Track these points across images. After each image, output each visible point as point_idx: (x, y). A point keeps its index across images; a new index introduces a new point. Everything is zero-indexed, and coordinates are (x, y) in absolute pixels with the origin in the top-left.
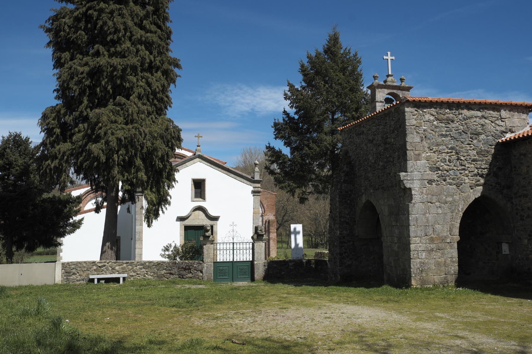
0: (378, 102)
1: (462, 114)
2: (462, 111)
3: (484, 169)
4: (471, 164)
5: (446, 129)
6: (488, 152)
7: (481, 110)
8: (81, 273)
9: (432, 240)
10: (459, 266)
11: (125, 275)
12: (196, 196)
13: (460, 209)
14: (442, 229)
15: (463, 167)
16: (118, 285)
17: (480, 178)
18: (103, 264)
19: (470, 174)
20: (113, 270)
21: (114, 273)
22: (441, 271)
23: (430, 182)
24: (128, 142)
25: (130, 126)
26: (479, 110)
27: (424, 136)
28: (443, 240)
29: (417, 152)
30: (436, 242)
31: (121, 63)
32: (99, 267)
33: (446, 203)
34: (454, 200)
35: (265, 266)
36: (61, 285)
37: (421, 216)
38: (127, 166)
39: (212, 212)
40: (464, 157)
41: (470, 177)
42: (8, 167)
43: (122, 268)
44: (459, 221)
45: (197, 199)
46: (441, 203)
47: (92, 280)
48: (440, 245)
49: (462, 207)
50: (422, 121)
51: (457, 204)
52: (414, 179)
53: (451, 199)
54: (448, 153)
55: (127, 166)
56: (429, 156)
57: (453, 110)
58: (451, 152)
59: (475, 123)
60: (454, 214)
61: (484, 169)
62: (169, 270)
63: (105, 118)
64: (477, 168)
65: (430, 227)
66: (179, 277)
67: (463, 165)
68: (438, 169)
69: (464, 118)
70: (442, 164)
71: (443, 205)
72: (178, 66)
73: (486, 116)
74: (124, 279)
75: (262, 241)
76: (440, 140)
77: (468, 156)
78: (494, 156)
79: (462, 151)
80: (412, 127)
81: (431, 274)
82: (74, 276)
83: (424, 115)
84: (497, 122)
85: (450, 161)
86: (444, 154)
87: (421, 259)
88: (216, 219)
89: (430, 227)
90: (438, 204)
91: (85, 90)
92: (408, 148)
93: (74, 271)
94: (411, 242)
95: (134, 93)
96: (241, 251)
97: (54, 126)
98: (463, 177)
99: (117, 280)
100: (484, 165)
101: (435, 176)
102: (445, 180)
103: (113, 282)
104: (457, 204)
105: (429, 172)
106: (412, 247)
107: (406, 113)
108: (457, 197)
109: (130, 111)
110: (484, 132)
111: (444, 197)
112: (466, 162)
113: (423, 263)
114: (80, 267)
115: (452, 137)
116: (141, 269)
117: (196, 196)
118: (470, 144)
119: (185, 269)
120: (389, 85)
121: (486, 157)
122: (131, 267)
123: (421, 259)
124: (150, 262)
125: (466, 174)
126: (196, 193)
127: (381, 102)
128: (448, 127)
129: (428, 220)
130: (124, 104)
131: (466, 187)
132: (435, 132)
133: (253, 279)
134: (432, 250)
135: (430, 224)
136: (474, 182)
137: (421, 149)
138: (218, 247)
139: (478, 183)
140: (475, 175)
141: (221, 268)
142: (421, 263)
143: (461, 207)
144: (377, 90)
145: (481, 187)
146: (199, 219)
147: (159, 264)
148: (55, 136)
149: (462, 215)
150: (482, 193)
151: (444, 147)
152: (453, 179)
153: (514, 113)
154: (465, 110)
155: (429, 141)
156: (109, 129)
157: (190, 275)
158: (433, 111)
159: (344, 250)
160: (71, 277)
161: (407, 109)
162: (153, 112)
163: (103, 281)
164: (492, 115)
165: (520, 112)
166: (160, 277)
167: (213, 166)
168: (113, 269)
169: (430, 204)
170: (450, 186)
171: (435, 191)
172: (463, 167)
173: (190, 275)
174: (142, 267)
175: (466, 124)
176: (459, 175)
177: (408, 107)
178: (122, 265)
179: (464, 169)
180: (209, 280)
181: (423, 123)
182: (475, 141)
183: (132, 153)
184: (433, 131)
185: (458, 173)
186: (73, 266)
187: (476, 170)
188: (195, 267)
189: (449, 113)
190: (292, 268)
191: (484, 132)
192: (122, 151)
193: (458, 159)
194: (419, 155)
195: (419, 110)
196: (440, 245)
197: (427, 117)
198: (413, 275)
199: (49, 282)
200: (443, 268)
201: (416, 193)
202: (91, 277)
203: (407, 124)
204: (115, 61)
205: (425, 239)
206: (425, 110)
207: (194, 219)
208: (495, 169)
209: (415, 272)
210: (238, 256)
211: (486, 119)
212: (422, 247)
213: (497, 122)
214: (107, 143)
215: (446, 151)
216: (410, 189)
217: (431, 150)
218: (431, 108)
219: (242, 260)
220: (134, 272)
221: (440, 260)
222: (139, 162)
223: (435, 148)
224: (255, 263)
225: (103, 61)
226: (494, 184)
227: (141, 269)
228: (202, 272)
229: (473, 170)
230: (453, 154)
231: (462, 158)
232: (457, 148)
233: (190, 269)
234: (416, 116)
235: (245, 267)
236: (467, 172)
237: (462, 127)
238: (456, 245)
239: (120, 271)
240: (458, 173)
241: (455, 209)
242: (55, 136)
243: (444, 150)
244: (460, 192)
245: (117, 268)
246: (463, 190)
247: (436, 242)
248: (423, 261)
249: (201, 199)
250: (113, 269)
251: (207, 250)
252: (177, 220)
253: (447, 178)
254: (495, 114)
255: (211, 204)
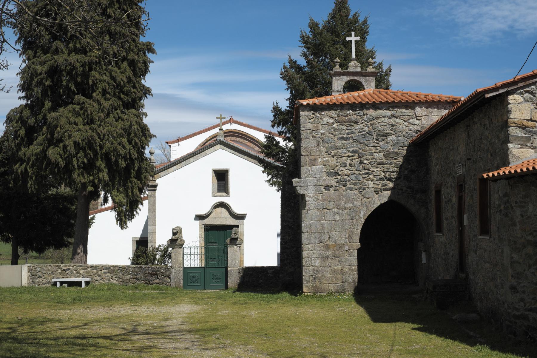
0: (334, 91)
1: (367, 114)
2: (368, 112)
3: (393, 172)
4: (377, 167)
5: (347, 131)
6: (397, 154)
7: (391, 109)
8: (47, 276)
9: (327, 247)
10: (358, 274)
11: (88, 279)
12: (219, 190)
13: (361, 216)
14: (339, 236)
15: (367, 171)
16: (79, 288)
17: (389, 182)
18: (67, 268)
19: (375, 179)
20: (78, 274)
21: (78, 277)
22: (337, 279)
23: (327, 188)
24: (86, 144)
25: (87, 127)
26: (388, 110)
27: (321, 141)
28: (340, 247)
29: (312, 157)
30: (332, 249)
31: (79, 60)
32: (64, 270)
33: (345, 209)
34: (355, 206)
35: (239, 273)
36: (27, 288)
37: (316, 222)
38: (89, 167)
39: (237, 210)
40: (368, 160)
41: (375, 182)
42: (6, 162)
43: (86, 272)
44: (360, 228)
45: (220, 194)
46: (339, 209)
47: (55, 284)
48: (337, 252)
49: (364, 214)
50: (319, 125)
51: (358, 210)
52: (309, 185)
53: (351, 205)
54: (349, 157)
55: (89, 167)
56: (326, 160)
57: (356, 111)
58: (352, 156)
59: (383, 124)
60: (355, 220)
61: (393, 172)
62: (135, 275)
63: (62, 121)
64: (384, 172)
65: (326, 234)
66: (146, 283)
67: (367, 169)
68: (337, 174)
69: (369, 119)
70: (342, 169)
71: (341, 211)
72: (152, 51)
73: (396, 115)
74: (87, 283)
75: (236, 245)
76: (339, 143)
77: (372, 159)
78: (406, 158)
79: (365, 154)
80: (308, 132)
81: (325, 282)
82: (40, 279)
83: (321, 119)
84: (411, 121)
85: (351, 165)
86: (344, 158)
87: (315, 266)
88: (242, 217)
89: (326, 234)
90: (335, 210)
91: (47, 90)
92: (302, 153)
93: (39, 274)
94: (304, 249)
95: (98, 89)
96: (193, 256)
97: (17, 129)
98: (366, 181)
99: (79, 284)
100: (393, 168)
101: (334, 182)
102: (344, 186)
103: (76, 286)
104: (358, 210)
105: (326, 177)
106: (305, 254)
107: (301, 118)
108: (358, 203)
109: (89, 112)
110: (393, 133)
111: (343, 203)
112: (370, 166)
113: (317, 271)
114: (45, 270)
115: (354, 140)
116: (106, 273)
117: (219, 190)
118: (376, 147)
119: (152, 275)
120: (353, 72)
121: (396, 159)
122: (95, 271)
123: (315, 266)
124: (115, 266)
125: (370, 178)
126: (219, 186)
127: (338, 91)
128: (350, 130)
129: (323, 227)
130: (84, 103)
131: (369, 192)
132: (334, 135)
133: (227, 287)
134: (327, 257)
135: (326, 231)
136: (380, 186)
137: (318, 153)
138: (185, 251)
139: (385, 187)
140: (382, 179)
141: (192, 274)
142: (314, 270)
143: (362, 213)
144: (334, 78)
145: (389, 192)
146: (222, 218)
147: (124, 269)
148: (19, 138)
149: (364, 221)
150: (390, 197)
151: (345, 151)
152: (355, 184)
153: (432, 110)
154: (371, 110)
155: (327, 145)
156: (66, 132)
157: (157, 281)
158: (333, 113)
159: (286, 257)
160: (37, 280)
161: (302, 113)
162: (119, 107)
163: (66, 285)
164: (404, 114)
165: (441, 108)
166: (126, 282)
167: (237, 153)
168: (78, 273)
169: (326, 210)
170: (351, 192)
171: (333, 197)
172: (367, 171)
173: (157, 281)
174: (107, 271)
175: (372, 125)
176: (362, 180)
177: (303, 111)
178: (86, 269)
179: (368, 173)
180: (177, 286)
181: (321, 127)
182: (382, 143)
183: (91, 155)
184: (332, 134)
185: (361, 177)
186: (38, 269)
187: (383, 174)
188: (163, 272)
189: (351, 114)
190: (271, 276)
191: (393, 133)
192: (81, 154)
193: (361, 163)
194: (315, 160)
195: (316, 114)
196: (337, 252)
197: (326, 120)
198: (305, 282)
199: (16, 284)
200: (340, 276)
201: (310, 199)
202: (54, 280)
203: (302, 129)
204: (74, 58)
205: (319, 247)
206: (322, 113)
207: (215, 218)
208: (406, 172)
209: (307, 279)
210: (189, 261)
211: (397, 118)
212: (317, 254)
213: (411, 121)
214: (65, 147)
215: (347, 155)
216: (303, 196)
217: (329, 154)
218: (330, 110)
219: (192, 266)
220: (99, 276)
221: (336, 268)
222: (100, 163)
223: (333, 153)
224: (229, 269)
225: (60, 59)
226: (404, 188)
227: (106, 273)
228: (170, 278)
229: (378, 173)
230: (356, 157)
231: (365, 162)
232: (360, 151)
233: (156, 274)
234: (312, 120)
235: (218, 274)
236: (371, 176)
237: (367, 129)
238: (356, 253)
239: (85, 275)
240: (361, 177)
241: (355, 216)
242: (19, 138)
243: (344, 153)
244: (362, 197)
245: (82, 272)
246: (366, 195)
247: (335, 250)
248: (316, 268)
249: (224, 194)
250: (78, 273)
251: (176, 255)
252: (195, 219)
253: (348, 183)
254: (408, 112)
255: (236, 200)
